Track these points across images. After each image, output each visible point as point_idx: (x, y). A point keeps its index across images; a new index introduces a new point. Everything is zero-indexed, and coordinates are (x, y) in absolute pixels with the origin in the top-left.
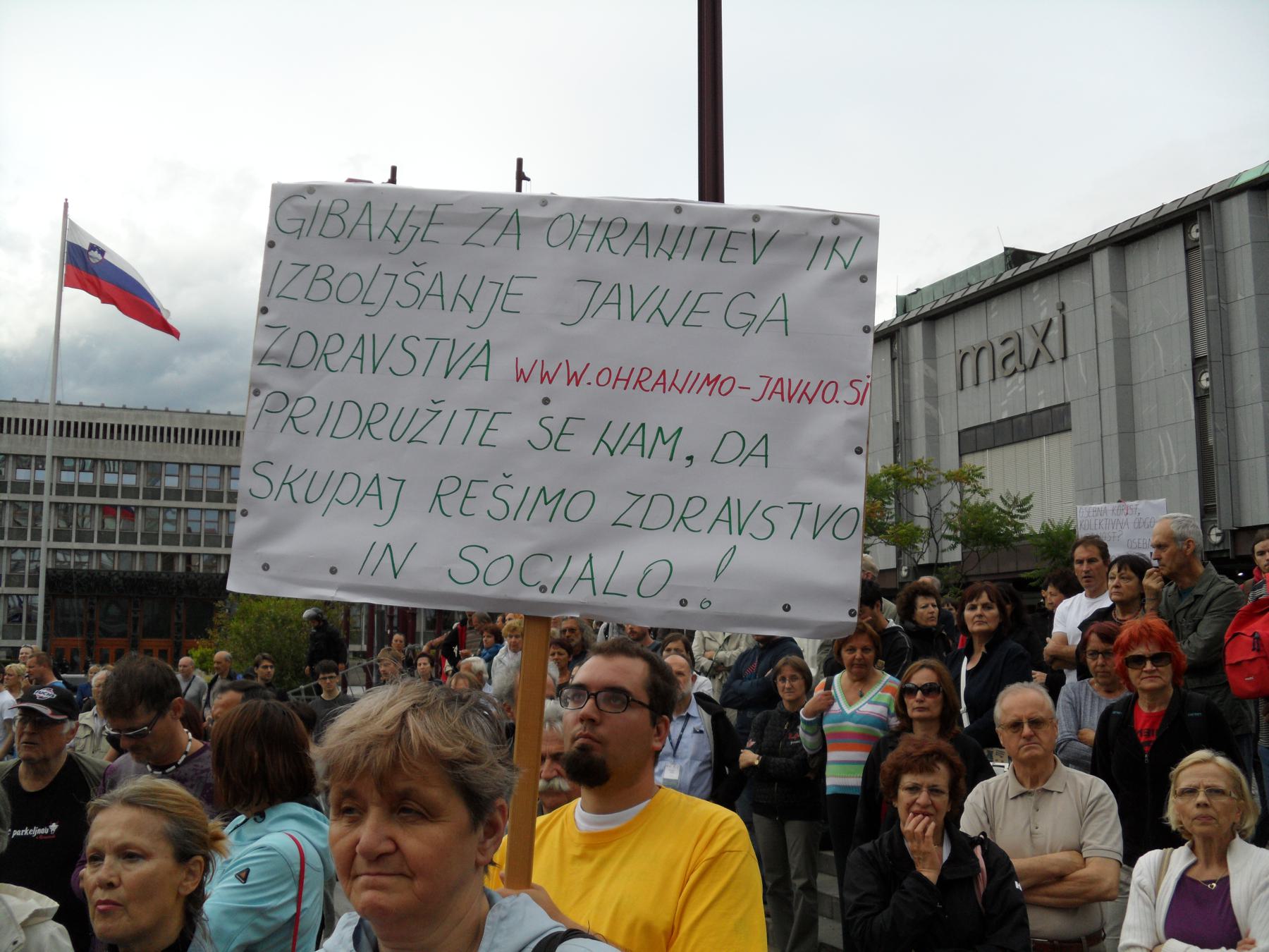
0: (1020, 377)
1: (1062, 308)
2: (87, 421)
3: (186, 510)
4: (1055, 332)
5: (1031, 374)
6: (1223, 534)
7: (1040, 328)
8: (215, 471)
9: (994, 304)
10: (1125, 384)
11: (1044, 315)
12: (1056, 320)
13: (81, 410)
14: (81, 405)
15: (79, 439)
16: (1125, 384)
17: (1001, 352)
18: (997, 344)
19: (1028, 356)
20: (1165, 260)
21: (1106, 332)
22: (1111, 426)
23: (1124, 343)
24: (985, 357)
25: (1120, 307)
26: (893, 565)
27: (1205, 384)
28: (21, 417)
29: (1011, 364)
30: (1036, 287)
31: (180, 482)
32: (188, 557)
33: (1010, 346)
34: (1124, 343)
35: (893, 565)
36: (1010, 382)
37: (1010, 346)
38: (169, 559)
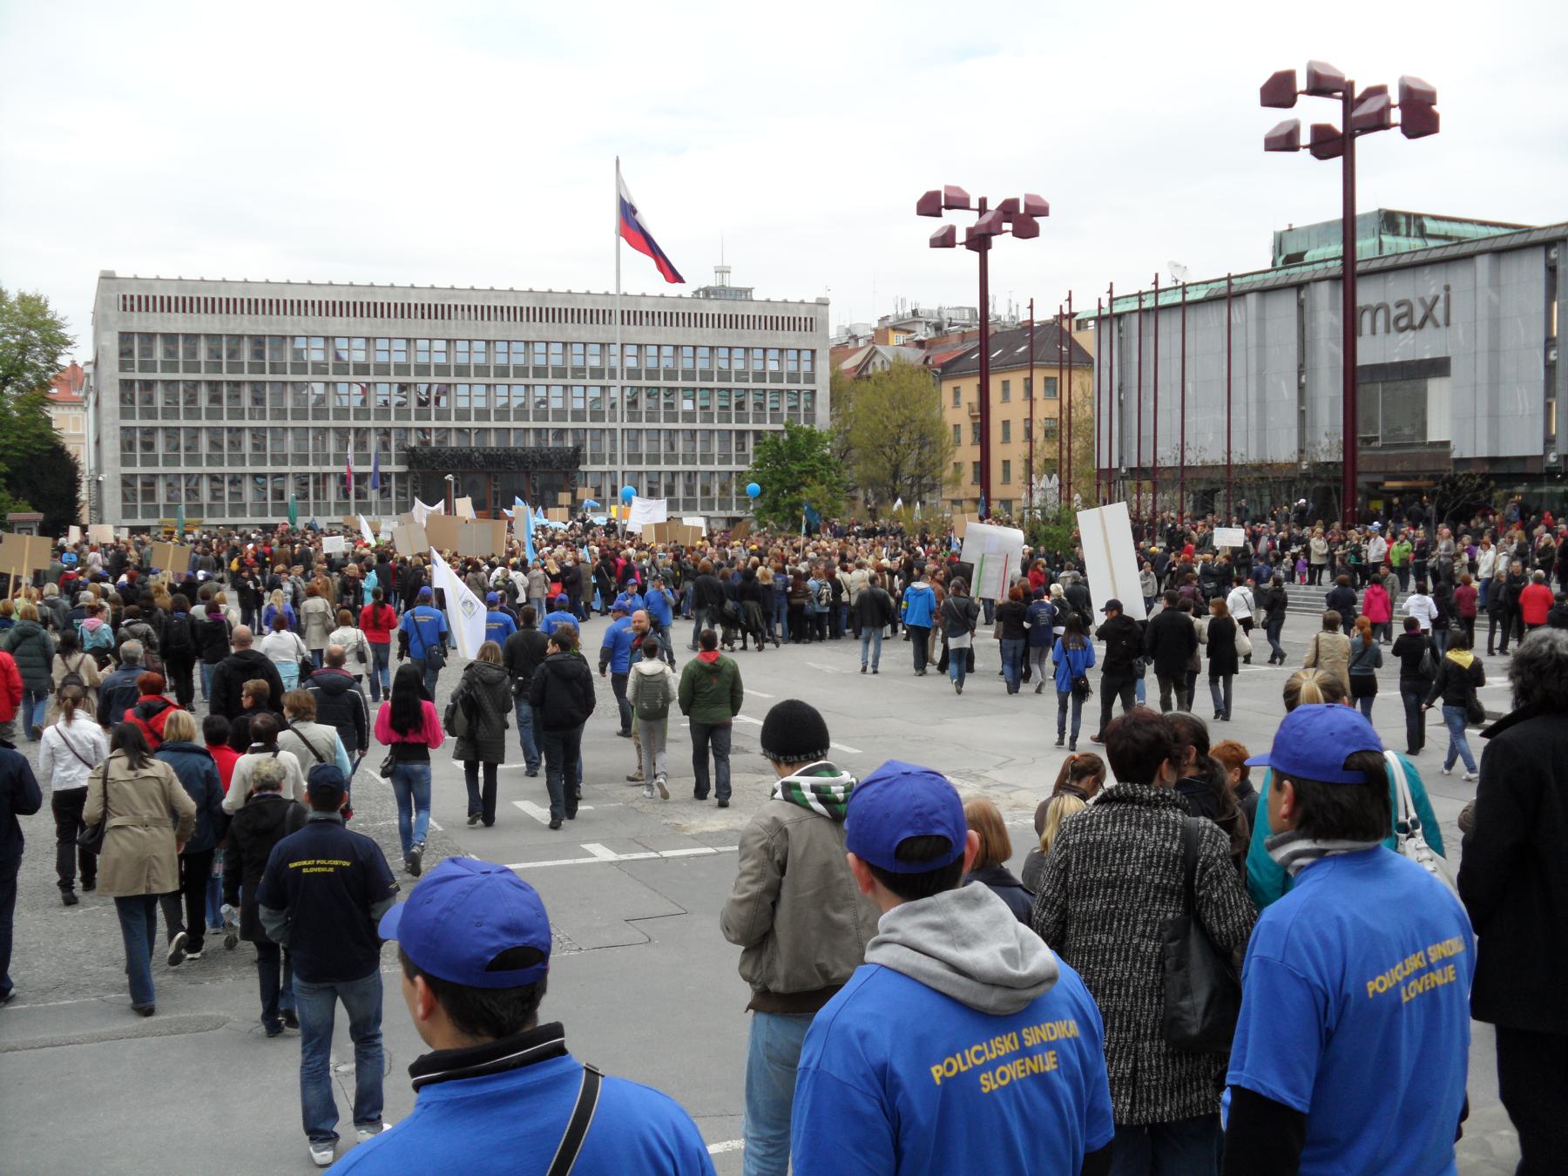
0: (1410, 334)
1: (1447, 288)
2: (439, 303)
3: (335, 384)
4: (1440, 305)
5: (1420, 334)
6: (1559, 457)
7: (1429, 301)
8: (402, 345)
9: (1391, 276)
10: (1495, 351)
11: (1433, 291)
12: (1442, 296)
13: (352, 290)
14: (351, 285)
15: (433, 320)
16: (1495, 351)
17: (1394, 313)
18: (1392, 307)
19: (1417, 322)
20: (1532, 268)
21: (1483, 312)
22: (1482, 377)
23: (1495, 322)
24: (1381, 315)
25: (1495, 298)
26: (1295, 459)
27: (1552, 357)
28: (379, 301)
29: (1403, 323)
30: (1427, 270)
31: (367, 356)
32: (538, 431)
33: (1403, 309)
34: (1495, 322)
35: (1295, 459)
36: (1402, 336)
37: (1403, 309)
38: (560, 433)
